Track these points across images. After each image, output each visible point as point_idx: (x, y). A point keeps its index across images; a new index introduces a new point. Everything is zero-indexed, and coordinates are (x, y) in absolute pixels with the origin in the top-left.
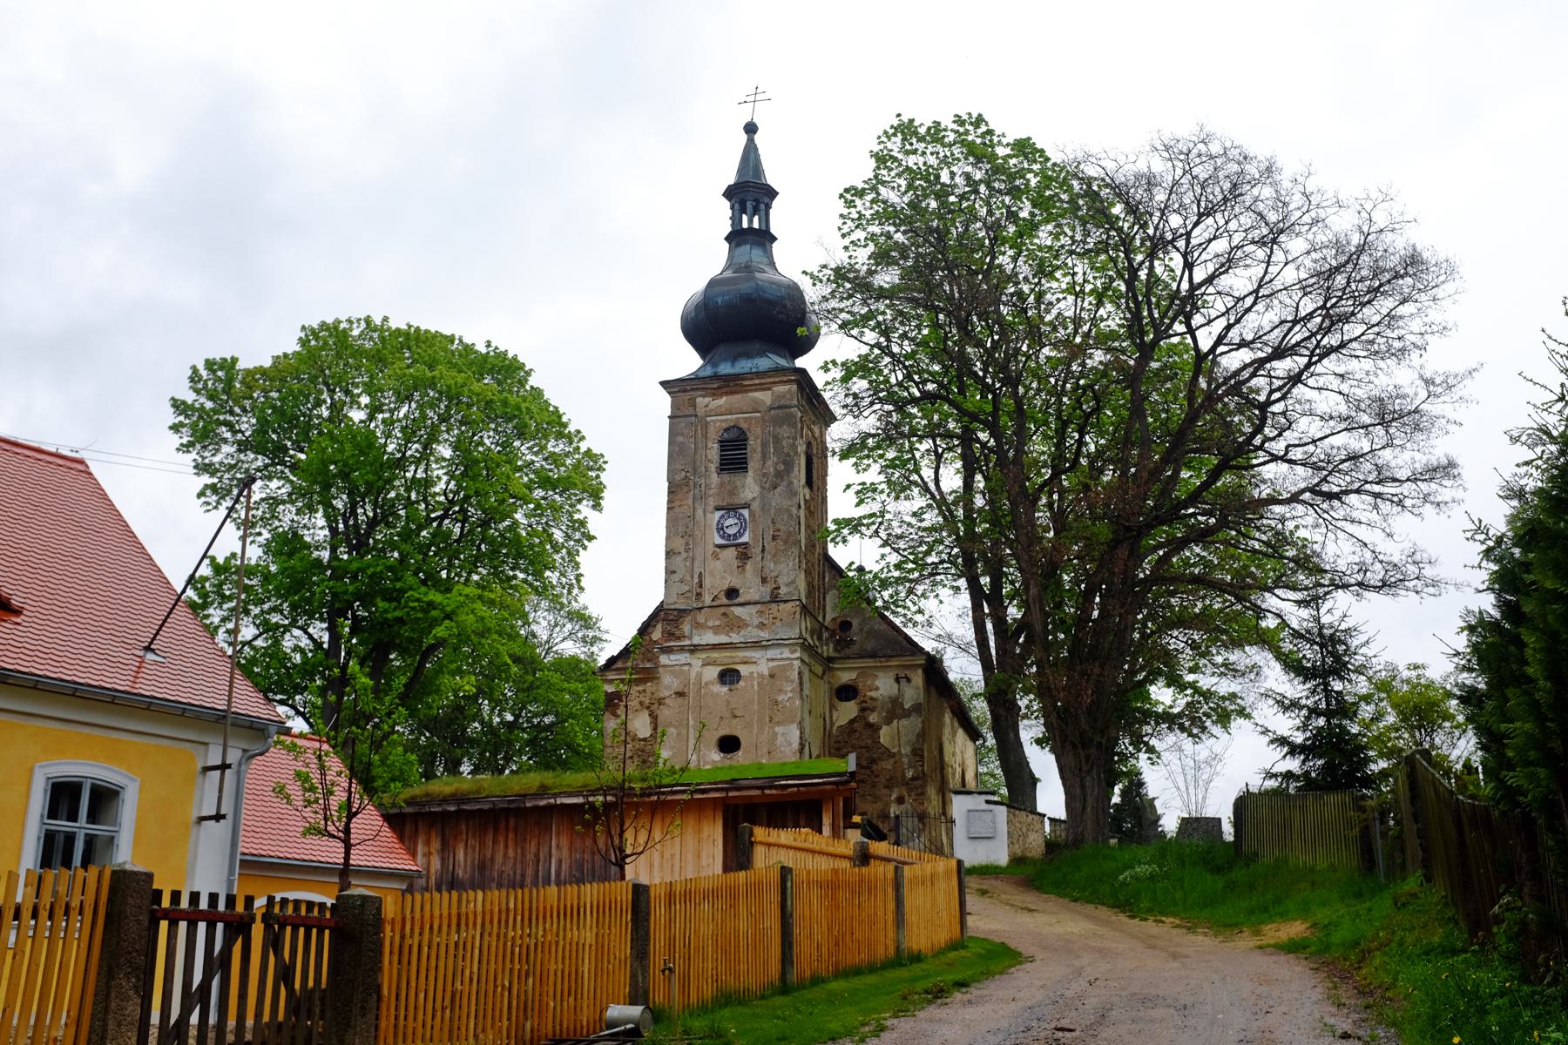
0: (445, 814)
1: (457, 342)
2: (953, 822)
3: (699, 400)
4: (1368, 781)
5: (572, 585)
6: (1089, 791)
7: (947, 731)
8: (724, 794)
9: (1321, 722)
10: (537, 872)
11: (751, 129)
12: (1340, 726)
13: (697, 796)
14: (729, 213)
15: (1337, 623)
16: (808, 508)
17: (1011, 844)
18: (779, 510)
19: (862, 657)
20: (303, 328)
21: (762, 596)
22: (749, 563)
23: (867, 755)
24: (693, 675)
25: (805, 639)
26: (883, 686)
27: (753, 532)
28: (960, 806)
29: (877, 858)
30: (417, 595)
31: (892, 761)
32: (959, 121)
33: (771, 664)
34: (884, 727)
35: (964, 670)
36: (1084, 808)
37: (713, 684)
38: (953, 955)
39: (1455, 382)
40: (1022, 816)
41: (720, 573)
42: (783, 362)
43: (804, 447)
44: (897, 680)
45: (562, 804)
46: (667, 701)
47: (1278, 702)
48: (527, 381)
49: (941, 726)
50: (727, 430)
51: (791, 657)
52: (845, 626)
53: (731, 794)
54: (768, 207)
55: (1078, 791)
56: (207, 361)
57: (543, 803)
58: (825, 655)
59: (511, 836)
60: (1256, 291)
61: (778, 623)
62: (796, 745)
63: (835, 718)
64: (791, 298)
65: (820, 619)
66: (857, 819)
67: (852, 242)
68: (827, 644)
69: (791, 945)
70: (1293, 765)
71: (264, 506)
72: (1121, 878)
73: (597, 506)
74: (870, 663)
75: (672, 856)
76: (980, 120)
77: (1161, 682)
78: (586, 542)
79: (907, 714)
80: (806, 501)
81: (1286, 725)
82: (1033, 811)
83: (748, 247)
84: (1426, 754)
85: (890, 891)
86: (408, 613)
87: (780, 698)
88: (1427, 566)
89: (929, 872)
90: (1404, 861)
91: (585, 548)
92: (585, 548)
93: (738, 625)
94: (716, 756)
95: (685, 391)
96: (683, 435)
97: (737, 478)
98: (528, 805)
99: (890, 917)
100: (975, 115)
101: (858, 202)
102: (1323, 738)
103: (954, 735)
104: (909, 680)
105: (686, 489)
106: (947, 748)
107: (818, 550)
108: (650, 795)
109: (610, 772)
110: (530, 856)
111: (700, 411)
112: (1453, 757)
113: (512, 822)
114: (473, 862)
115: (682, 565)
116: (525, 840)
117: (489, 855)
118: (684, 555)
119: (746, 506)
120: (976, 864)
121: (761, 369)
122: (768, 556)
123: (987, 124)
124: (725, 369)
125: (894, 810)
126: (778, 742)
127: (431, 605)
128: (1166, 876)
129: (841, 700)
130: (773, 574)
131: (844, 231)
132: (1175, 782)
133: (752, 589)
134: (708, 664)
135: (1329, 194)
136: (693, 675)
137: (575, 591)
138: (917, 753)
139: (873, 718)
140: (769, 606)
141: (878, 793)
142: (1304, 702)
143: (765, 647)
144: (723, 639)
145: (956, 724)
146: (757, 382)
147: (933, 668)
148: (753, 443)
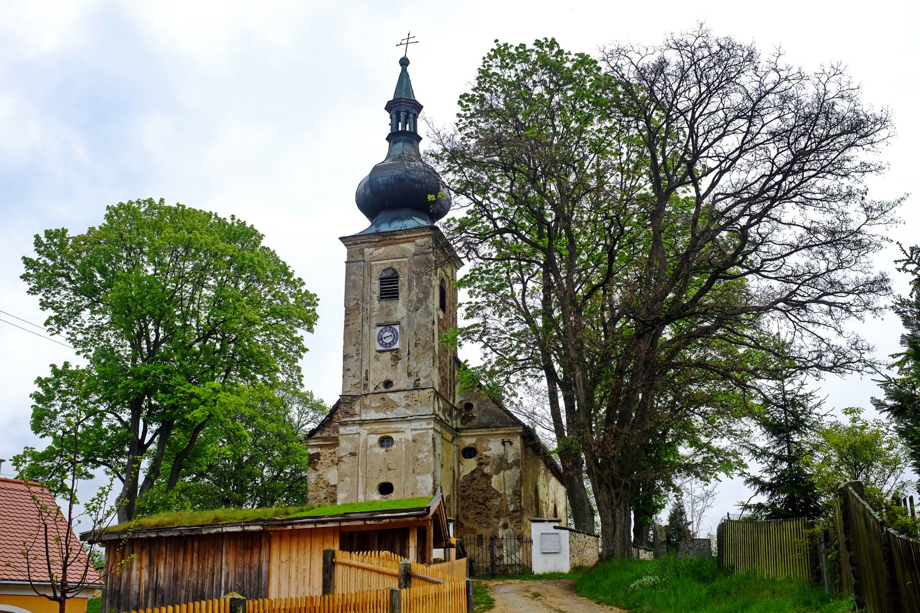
0: (149, 539)
1: (213, 217)
3: (366, 250)
4: (818, 512)
6: (618, 520)
7: (541, 481)
8: (338, 524)
9: (785, 465)
11: (404, 62)
12: (798, 468)
14: (390, 121)
15: (796, 390)
18: (419, 326)
19: (479, 428)
20: (108, 208)
22: (400, 362)
23: (483, 495)
24: (362, 440)
26: (494, 448)
30: (182, 389)
31: (499, 499)
32: (538, 43)
33: (414, 433)
34: (495, 476)
35: (547, 436)
36: (614, 532)
37: (375, 446)
39: (888, 209)
41: (379, 371)
42: (424, 223)
43: (438, 282)
44: (503, 443)
46: (344, 459)
47: (752, 451)
48: (260, 242)
50: (385, 270)
51: (428, 427)
53: (343, 524)
56: (46, 231)
57: (214, 531)
58: (455, 427)
59: (195, 555)
60: (741, 148)
61: (419, 404)
62: (430, 489)
63: (461, 470)
65: (451, 402)
67: (466, 134)
68: (456, 419)
70: (763, 499)
71: (92, 331)
72: (632, 586)
73: (310, 330)
74: (485, 432)
75: (304, 570)
76: (553, 43)
77: (686, 442)
78: (302, 353)
79: (510, 467)
80: (439, 320)
81: (756, 468)
84: (859, 487)
86: (177, 401)
87: (419, 456)
88: (867, 352)
90: (841, 582)
91: (301, 357)
92: (301, 357)
93: (393, 406)
94: (377, 497)
95: (357, 244)
96: (355, 274)
97: (391, 304)
98: (204, 533)
100: (549, 40)
102: (786, 478)
103: (548, 481)
104: (511, 443)
105: (357, 312)
106: (542, 491)
108: (286, 525)
110: (208, 570)
111: (367, 258)
112: (884, 491)
113: (196, 545)
115: (354, 365)
116: (204, 558)
117: (180, 570)
118: (356, 358)
119: (398, 323)
120: (547, 571)
121: (408, 227)
122: (412, 358)
123: (558, 47)
124: (384, 228)
125: (501, 533)
127: (192, 395)
128: (665, 585)
129: (465, 457)
133: (401, 382)
134: (372, 433)
135: (794, 70)
136: (362, 440)
138: (517, 493)
139: (487, 470)
141: (490, 521)
142: (771, 450)
143: (410, 421)
145: (550, 474)
147: (529, 436)
148: (403, 280)
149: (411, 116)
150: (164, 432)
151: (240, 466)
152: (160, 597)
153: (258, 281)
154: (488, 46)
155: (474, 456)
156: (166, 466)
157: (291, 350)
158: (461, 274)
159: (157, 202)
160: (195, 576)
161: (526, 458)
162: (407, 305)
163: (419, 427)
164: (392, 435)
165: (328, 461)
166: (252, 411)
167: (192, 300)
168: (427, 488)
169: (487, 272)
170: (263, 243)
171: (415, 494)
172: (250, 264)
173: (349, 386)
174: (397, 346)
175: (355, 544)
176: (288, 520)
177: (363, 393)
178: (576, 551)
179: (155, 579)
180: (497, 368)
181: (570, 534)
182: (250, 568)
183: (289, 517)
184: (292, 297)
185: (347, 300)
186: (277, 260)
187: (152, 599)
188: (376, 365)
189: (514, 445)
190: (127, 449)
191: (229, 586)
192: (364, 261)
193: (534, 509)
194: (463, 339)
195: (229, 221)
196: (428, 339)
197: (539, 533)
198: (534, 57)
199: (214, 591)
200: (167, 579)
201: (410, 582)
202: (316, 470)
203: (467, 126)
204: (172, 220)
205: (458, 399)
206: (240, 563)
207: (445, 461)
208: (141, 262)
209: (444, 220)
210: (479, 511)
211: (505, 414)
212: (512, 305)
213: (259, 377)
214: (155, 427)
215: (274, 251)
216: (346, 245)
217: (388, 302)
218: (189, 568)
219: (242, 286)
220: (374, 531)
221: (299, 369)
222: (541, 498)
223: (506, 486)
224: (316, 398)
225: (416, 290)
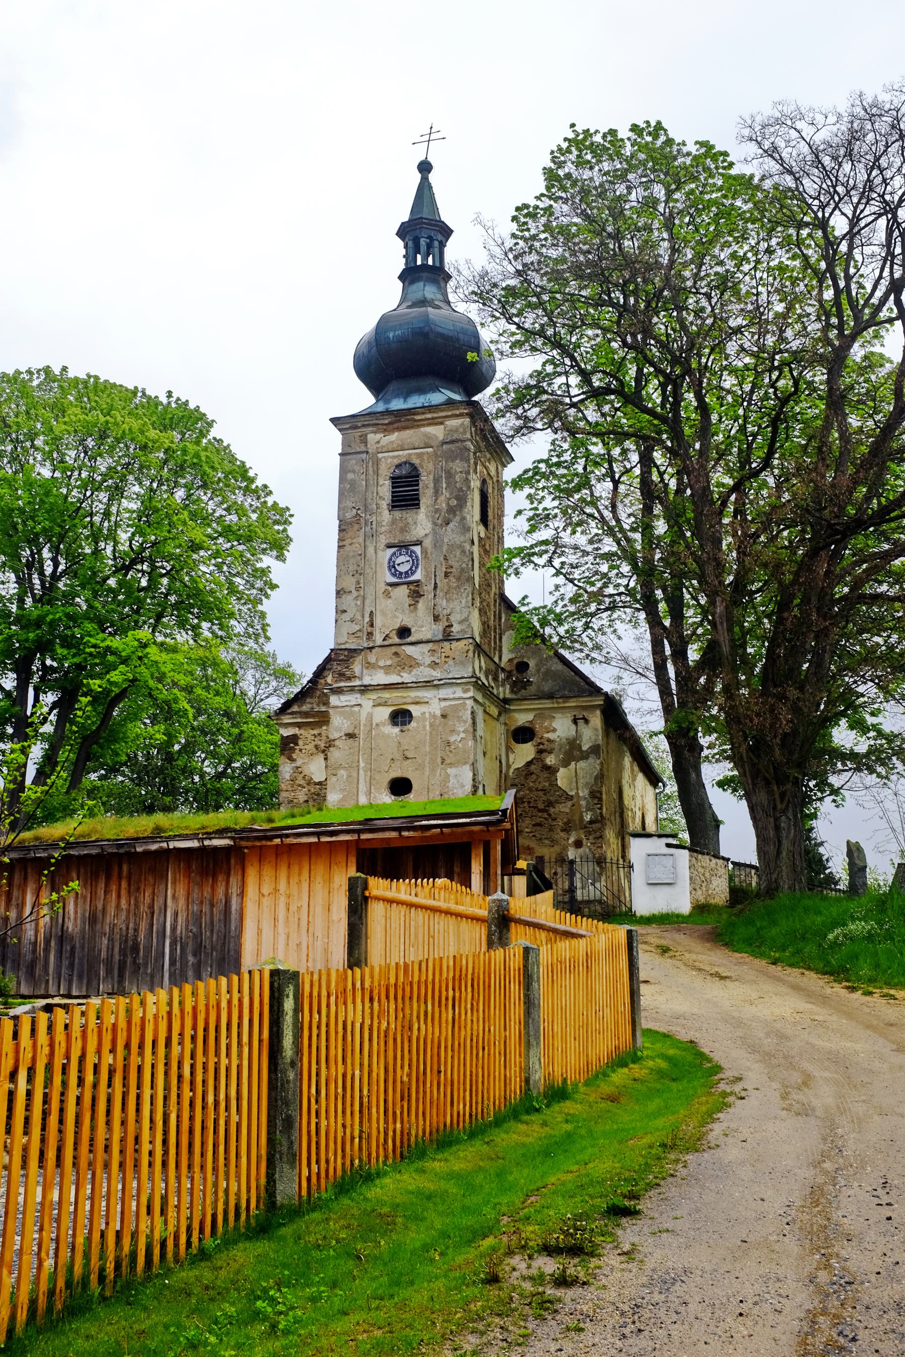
1: (140, 394)
2: (631, 867)
3: (371, 437)
5: (258, 635)
6: (784, 834)
8: (355, 837)
10: (152, 925)
11: (425, 167)
13: (325, 839)
14: (404, 252)
16: (482, 545)
18: (452, 547)
19: (540, 698)
21: (434, 635)
22: (421, 601)
23: (544, 798)
25: (479, 679)
28: (638, 849)
29: (519, 921)
30: (93, 641)
31: (570, 803)
32: (635, 128)
33: (443, 704)
34: (562, 770)
36: (779, 853)
37: (384, 724)
38: (620, 1076)
40: (705, 860)
42: (457, 397)
44: (575, 721)
45: (175, 848)
48: (208, 431)
49: (620, 768)
50: (398, 466)
51: (465, 696)
52: (522, 667)
54: (442, 245)
55: (772, 833)
57: (154, 847)
58: (501, 696)
59: (124, 884)
61: (451, 662)
62: (469, 787)
63: (511, 760)
64: (464, 331)
65: (496, 659)
66: (522, 864)
68: (503, 685)
69: (289, 1123)
72: (831, 937)
73: (281, 558)
74: (547, 704)
75: (299, 908)
79: (584, 756)
80: (480, 539)
82: (717, 856)
85: (515, 990)
86: (85, 659)
87: (452, 739)
89: (582, 952)
91: (267, 596)
92: (267, 596)
93: (410, 664)
94: (387, 798)
95: (356, 427)
96: (354, 471)
97: (408, 515)
98: (139, 849)
99: (514, 1030)
100: (653, 124)
101: (531, 224)
103: (634, 779)
104: (587, 721)
105: (356, 527)
106: (627, 792)
107: (494, 590)
108: (271, 838)
109: (281, 818)
110: (144, 908)
111: (372, 448)
113: (125, 868)
114: (83, 915)
115: (353, 604)
116: (138, 889)
117: (100, 906)
118: (355, 594)
119: (419, 543)
120: (656, 912)
121: (433, 403)
123: (666, 134)
124: (397, 404)
126: (450, 785)
127: (108, 649)
129: (517, 741)
130: (445, 612)
132: (889, 822)
133: (424, 629)
134: (380, 705)
137: (261, 640)
138: (596, 795)
139: (550, 760)
140: (442, 644)
144: (394, 679)
145: (636, 768)
146: (429, 416)
148: (426, 480)
149: (436, 244)
150: (65, 706)
151: (169, 758)
152: (68, 948)
153: (204, 486)
154: (558, 136)
155: (531, 739)
156: (65, 754)
157: (253, 586)
158: (510, 473)
159: (57, 371)
160: (123, 917)
161: (608, 743)
162: (433, 517)
163: (451, 696)
164: (411, 708)
165: (310, 747)
166: (189, 679)
167: (107, 514)
168: (463, 786)
169: (558, 465)
170: (214, 433)
171: (446, 796)
172: (195, 461)
173: (346, 635)
174: (417, 576)
175: (379, 868)
176: (273, 829)
177: (366, 645)
178: (698, 881)
179: (60, 921)
180: (572, 609)
181: (691, 856)
182: (212, 905)
183: (274, 825)
184: (254, 511)
185: (341, 509)
186: (232, 459)
187: (56, 952)
188: (386, 605)
189: (591, 724)
190: (10, 730)
191: (178, 932)
192: (367, 452)
193: (618, 819)
194: (523, 565)
195: (164, 400)
196: (464, 565)
197: (644, 854)
198: (628, 150)
199: (155, 940)
200: (79, 921)
201: (508, 930)
202: (292, 760)
203: (525, 252)
204: (79, 398)
205: (506, 656)
206: (195, 896)
207: (489, 747)
208: (31, 461)
209: (490, 390)
210: (538, 820)
211: (577, 678)
212: (591, 516)
213: (205, 625)
214: (50, 698)
215: (229, 445)
216: (340, 430)
217: (404, 512)
218: (113, 904)
219: (180, 494)
220: (407, 848)
221: (263, 615)
222: (626, 802)
223: (580, 785)
224: (281, 661)
225: (446, 494)
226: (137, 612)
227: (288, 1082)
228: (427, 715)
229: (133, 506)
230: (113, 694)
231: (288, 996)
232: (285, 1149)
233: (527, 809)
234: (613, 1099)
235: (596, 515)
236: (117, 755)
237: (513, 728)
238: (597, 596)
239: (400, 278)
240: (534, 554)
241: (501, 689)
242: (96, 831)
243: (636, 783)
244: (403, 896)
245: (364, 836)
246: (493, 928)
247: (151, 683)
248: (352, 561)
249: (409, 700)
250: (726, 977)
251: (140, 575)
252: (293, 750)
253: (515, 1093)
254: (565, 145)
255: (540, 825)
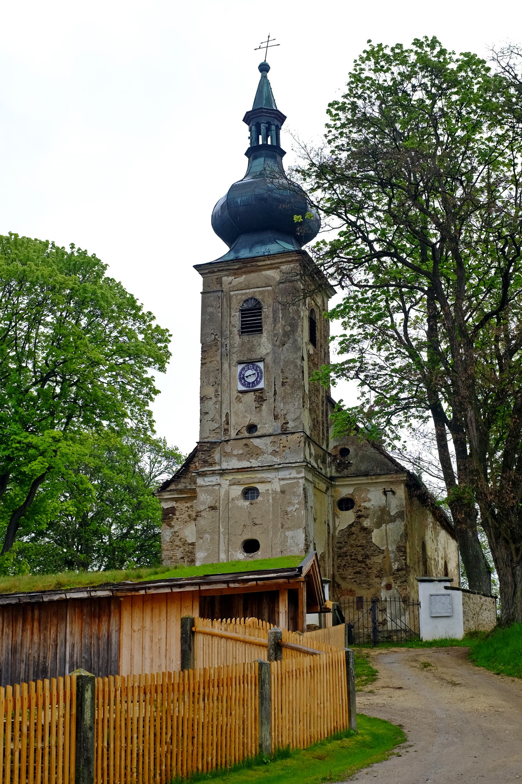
1: (50, 246)
3: (225, 279)
5: (146, 429)
7: (429, 534)
8: (196, 588)
11: (264, 68)
13: (176, 590)
14: (248, 134)
17: (466, 620)
18: (287, 363)
21: (274, 430)
24: (223, 492)
27: (268, 380)
30: (18, 438)
31: (382, 556)
32: (417, 43)
33: (282, 483)
34: (375, 530)
36: (515, 593)
37: (238, 499)
42: (290, 247)
43: (307, 313)
44: (385, 493)
45: (70, 598)
48: (103, 273)
50: (246, 301)
54: (278, 129)
55: (510, 579)
57: (56, 598)
59: (36, 625)
61: (287, 451)
62: (302, 546)
63: (337, 524)
65: (324, 447)
69: (88, 762)
73: (162, 369)
74: (363, 480)
75: (160, 640)
76: (433, 44)
78: (153, 396)
79: (392, 520)
80: (309, 355)
83: (262, 159)
86: (13, 452)
87: (289, 509)
91: (152, 399)
92: (152, 399)
93: (257, 453)
94: (241, 555)
95: (214, 272)
96: (212, 306)
97: (254, 339)
98: (46, 599)
100: (430, 38)
103: (437, 535)
104: (394, 493)
105: (215, 348)
108: (138, 590)
110: (50, 642)
111: (225, 287)
113: (36, 613)
115: (213, 408)
116: (46, 628)
117: (19, 641)
118: (214, 399)
119: (262, 360)
121: (272, 252)
123: (440, 45)
124: (244, 254)
127: (30, 446)
129: (341, 509)
131: (330, 138)
134: (234, 484)
138: (401, 550)
139: (367, 523)
141: (371, 581)
144: (245, 464)
146: (268, 262)
148: (267, 311)
149: (273, 128)
151: (84, 523)
153: (102, 316)
155: (352, 507)
157: (140, 392)
160: (36, 649)
162: (273, 340)
163: (288, 477)
164: (258, 486)
165: (185, 516)
166: (97, 461)
167: (28, 339)
168: (298, 545)
169: (363, 300)
170: (107, 274)
172: (93, 297)
173: (208, 431)
174: (261, 385)
175: (217, 610)
177: (223, 439)
178: (471, 614)
181: (464, 595)
182: (98, 639)
184: (141, 333)
186: (123, 293)
189: (397, 494)
191: (75, 658)
192: (222, 291)
193: (421, 567)
194: (337, 377)
195: (68, 250)
196: (296, 377)
199: (58, 665)
202: (171, 527)
203: (337, 137)
205: (332, 444)
206: (87, 632)
207: (318, 514)
209: (312, 243)
210: (358, 569)
212: (392, 336)
213: (105, 423)
215: (120, 283)
216: (201, 274)
217: (251, 336)
218: (29, 639)
219: (84, 322)
220: (239, 595)
222: (429, 553)
223: (389, 541)
224: (170, 445)
226: (52, 414)
227: (88, 738)
228: (270, 492)
229: (48, 331)
230: (35, 478)
231: (87, 690)
232: (86, 776)
233: (350, 561)
234: (320, 758)
235: (396, 336)
236: (40, 524)
237: (338, 499)
238: (396, 399)
239: (247, 154)
240: (344, 369)
241: (328, 469)
242: (15, 587)
243: (439, 539)
244: (216, 631)
245: (203, 588)
246: (271, 651)
247: (63, 469)
248: (212, 375)
249: (256, 480)
250: (458, 684)
251: (55, 384)
252: (171, 519)
253: (251, 753)
254: (365, 55)
255: (359, 573)
